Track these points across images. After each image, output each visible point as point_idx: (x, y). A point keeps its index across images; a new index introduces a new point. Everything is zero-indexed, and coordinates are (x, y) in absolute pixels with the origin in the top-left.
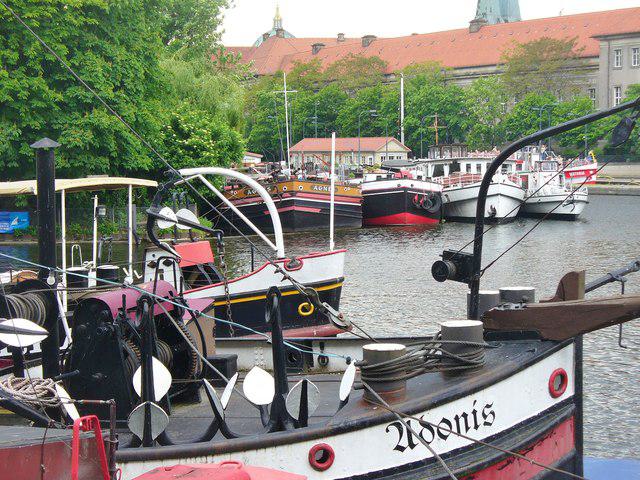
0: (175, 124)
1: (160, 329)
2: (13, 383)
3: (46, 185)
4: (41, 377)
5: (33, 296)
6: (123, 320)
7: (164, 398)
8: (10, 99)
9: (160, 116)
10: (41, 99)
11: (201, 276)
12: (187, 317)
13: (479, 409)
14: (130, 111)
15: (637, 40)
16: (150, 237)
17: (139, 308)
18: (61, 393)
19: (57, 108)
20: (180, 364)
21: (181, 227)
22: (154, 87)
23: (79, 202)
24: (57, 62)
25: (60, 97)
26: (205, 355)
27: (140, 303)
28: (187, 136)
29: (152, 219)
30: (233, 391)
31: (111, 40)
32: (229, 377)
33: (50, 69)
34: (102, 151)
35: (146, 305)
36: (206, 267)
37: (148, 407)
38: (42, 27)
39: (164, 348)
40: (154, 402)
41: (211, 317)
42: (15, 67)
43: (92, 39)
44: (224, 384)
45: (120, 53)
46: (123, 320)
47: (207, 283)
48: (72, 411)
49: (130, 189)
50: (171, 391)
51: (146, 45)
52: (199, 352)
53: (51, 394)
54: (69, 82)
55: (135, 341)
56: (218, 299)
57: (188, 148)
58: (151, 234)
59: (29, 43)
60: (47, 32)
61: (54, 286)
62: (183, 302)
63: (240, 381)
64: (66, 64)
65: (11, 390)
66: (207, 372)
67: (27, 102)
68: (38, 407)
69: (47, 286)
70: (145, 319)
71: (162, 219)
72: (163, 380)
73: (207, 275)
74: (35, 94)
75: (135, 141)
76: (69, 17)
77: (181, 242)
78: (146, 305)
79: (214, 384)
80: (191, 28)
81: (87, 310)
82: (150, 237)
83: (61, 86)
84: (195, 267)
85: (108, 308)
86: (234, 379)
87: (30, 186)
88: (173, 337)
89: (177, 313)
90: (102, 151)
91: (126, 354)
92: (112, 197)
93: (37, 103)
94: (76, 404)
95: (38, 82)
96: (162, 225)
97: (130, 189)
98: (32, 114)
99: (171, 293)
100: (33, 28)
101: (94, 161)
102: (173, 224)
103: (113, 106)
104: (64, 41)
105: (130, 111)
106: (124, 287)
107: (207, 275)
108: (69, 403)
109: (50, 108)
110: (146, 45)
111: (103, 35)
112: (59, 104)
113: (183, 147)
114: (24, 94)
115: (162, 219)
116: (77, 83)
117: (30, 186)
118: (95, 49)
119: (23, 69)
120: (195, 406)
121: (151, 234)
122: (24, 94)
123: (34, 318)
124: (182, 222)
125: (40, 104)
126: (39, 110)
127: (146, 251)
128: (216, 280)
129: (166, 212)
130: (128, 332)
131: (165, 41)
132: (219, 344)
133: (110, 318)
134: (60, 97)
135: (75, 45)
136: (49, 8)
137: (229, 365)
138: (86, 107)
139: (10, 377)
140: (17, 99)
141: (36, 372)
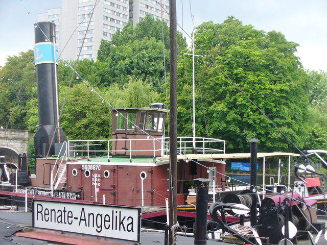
0: (313, 133)
1: (294, 211)
2: (239, 227)
3: (254, 155)
4: (250, 226)
5: (248, 197)
6: (279, 207)
7: (294, 237)
8: (252, 122)
9: (307, 128)
10: (264, 123)
11: (315, 191)
12: (305, 208)
13: (67, 210)
14: (296, 127)
15: (1, 193)
16: (296, 175)
17: (284, 203)
18: (255, 234)
19: (270, 126)
20: (301, 225)
21: (307, 172)
22: (305, 117)
23: (272, 162)
24: (271, 109)
25: (271, 122)
26: (311, 223)
27: (285, 201)
28: (317, 137)
29: (296, 169)
30: (321, 237)
31: (291, 102)
32: (319, 231)
33: (268, 112)
34: (285, 141)
35: (287, 202)
36: (317, 188)
37: (285, 241)
38: (265, 97)
39: (296, 218)
40: (289, 238)
41: (315, 208)
42: (255, 111)
43: (283, 101)
44: (317, 233)
45: (294, 106)
46: (279, 207)
47: (317, 194)
48: (259, 241)
49: (290, 157)
50: (297, 234)
51: (303, 103)
52: (309, 222)
53: (252, 233)
54: (275, 116)
55: (283, 215)
56: (319, 200)
57: (318, 142)
58: (296, 175)
59: (260, 103)
60: (267, 99)
61: (256, 192)
62: (303, 201)
63: (323, 233)
64: (274, 110)
65: (238, 230)
66: (311, 229)
67: (259, 124)
68: (247, 237)
69: (253, 192)
70: (287, 207)
71: (300, 169)
72: (293, 230)
73: (317, 190)
74: (262, 121)
75: (298, 138)
76: (275, 93)
77: (307, 177)
78: (287, 202)
79: (312, 234)
80: (321, 97)
81: (268, 202)
82: (296, 175)
83: (271, 118)
84: (313, 188)
85: (273, 202)
86: (321, 231)
87: (248, 155)
88: (298, 214)
89: (301, 205)
90: (285, 141)
91: (280, 220)
92: (285, 159)
93: (262, 124)
94: (261, 239)
95: (263, 117)
96: (300, 171)
97: (290, 157)
98: (261, 128)
99: (299, 197)
100: (262, 98)
101: (281, 145)
102: (304, 171)
103: (289, 125)
104: (273, 102)
105: (296, 127)
106: (281, 194)
107: (317, 190)
108: (258, 238)
109: (267, 126)
110: (303, 103)
111: (287, 99)
112: (271, 124)
113: (316, 141)
114: (258, 121)
115: (300, 169)
116: (277, 117)
117: (248, 155)
118: (284, 104)
119: (258, 112)
120: (307, 241)
121: (296, 175)
122: (258, 121)
123: (247, 205)
124: (308, 170)
125: (264, 125)
126: (264, 127)
127: (294, 180)
128: (321, 192)
129: (302, 166)
130: (281, 211)
131: (311, 101)
132: (319, 218)
133: (274, 206)
134: (271, 122)
135: (277, 103)
136: (268, 91)
137: (322, 226)
138: (279, 125)
139: (238, 225)
140: (255, 123)
141: (248, 224)
